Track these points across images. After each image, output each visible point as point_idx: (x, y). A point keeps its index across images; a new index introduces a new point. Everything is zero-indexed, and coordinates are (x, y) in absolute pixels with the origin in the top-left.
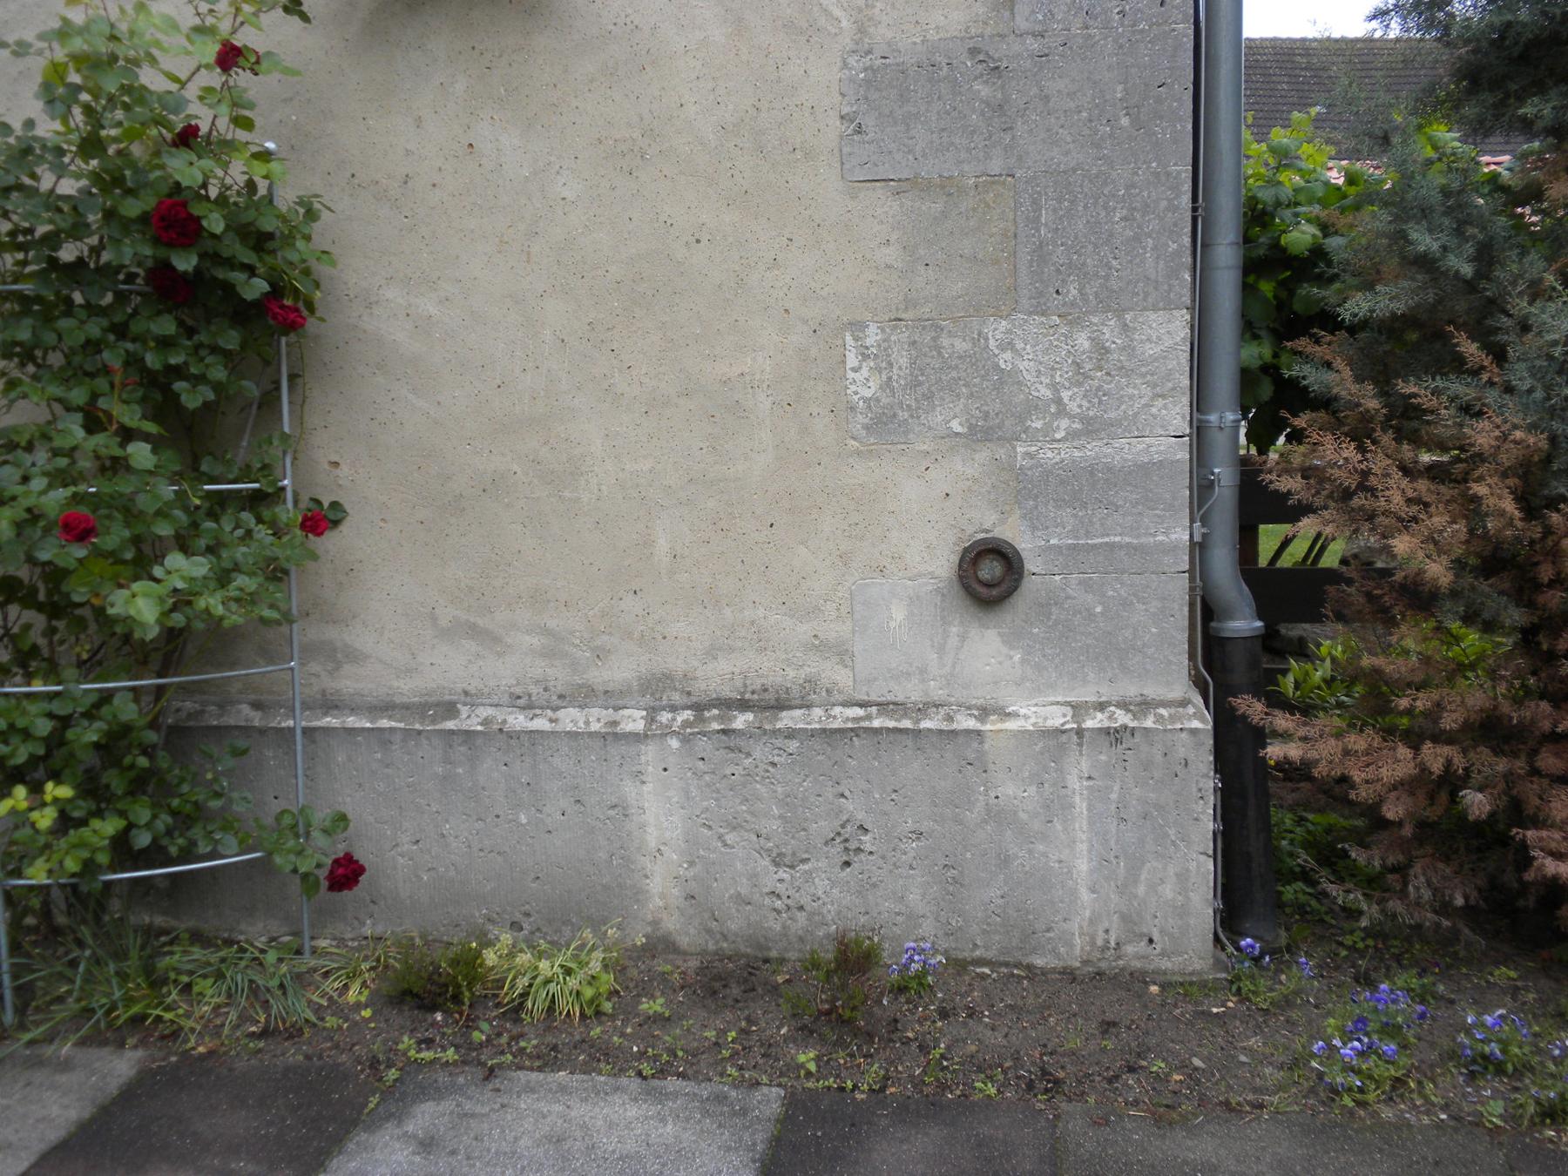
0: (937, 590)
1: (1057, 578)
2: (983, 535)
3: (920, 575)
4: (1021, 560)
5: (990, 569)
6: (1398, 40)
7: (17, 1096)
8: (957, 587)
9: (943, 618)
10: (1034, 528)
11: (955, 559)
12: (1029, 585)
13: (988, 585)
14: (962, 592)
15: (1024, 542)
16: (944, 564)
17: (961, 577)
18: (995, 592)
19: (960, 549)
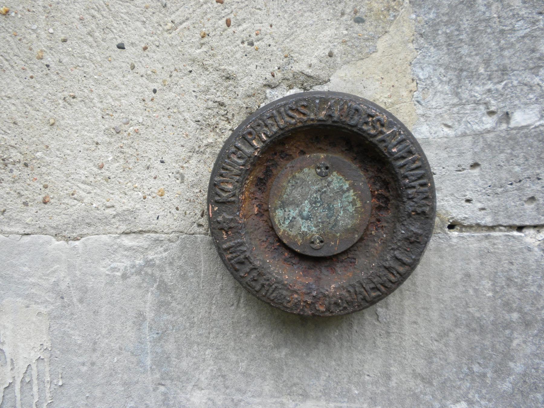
0: (146, 271)
1: (530, 238)
2: (312, 122)
3: (90, 222)
4: (425, 175)
5: (319, 201)
6: (329, 125)
7: (258, 170)
8: (206, 261)
9: (162, 361)
10: (462, 73)
11: (202, 170)
12: (446, 258)
13: (312, 260)
14: (223, 281)
15: (433, 121)
16: (165, 184)
17: (216, 229)
18: (334, 283)
19: (217, 140)
